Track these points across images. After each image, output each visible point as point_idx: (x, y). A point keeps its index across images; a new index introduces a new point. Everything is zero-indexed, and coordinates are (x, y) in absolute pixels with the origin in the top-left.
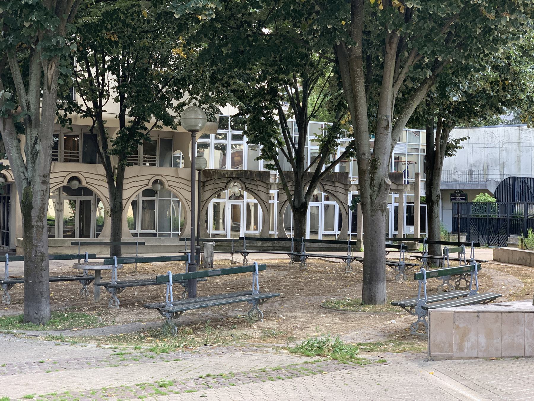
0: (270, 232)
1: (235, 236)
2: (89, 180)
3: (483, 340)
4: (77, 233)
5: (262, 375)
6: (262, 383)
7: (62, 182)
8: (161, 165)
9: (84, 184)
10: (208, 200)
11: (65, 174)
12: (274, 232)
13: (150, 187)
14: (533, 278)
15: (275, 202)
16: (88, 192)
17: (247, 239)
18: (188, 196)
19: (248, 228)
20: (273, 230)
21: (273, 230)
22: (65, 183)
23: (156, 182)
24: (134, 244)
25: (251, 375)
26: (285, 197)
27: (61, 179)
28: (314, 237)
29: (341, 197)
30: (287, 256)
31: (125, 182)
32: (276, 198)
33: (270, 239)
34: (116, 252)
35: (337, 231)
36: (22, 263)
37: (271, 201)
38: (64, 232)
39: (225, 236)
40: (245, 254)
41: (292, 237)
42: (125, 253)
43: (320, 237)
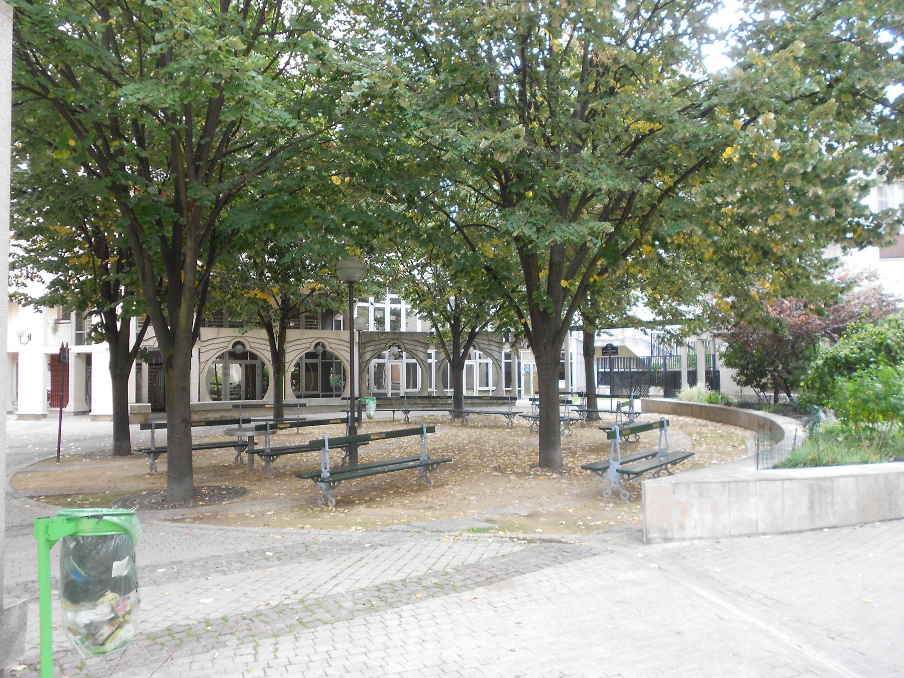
0: (429, 390)
1: (395, 394)
2: (252, 345)
3: (708, 517)
4: (243, 395)
5: (442, 585)
6: (445, 597)
7: (227, 347)
8: (323, 328)
9: (248, 348)
10: (369, 361)
11: (229, 339)
12: (433, 390)
13: (312, 349)
14: (902, 455)
15: (433, 361)
16: (254, 357)
17: (408, 397)
18: (348, 356)
19: (408, 387)
20: (431, 387)
21: (431, 387)
22: (230, 348)
23: (318, 344)
24: (296, 405)
25: (426, 583)
26: (443, 356)
27: (226, 344)
28: (470, 394)
29: (496, 355)
30: (448, 413)
31: (286, 345)
32: (433, 356)
33: (430, 397)
34: (278, 414)
35: (491, 387)
36: (166, 430)
37: (429, 361)
38: (231, 394)
39: (386, 394)
40: (406, 412)
41: (452, 394)
42: (288, 415)
43: (476, 394)
